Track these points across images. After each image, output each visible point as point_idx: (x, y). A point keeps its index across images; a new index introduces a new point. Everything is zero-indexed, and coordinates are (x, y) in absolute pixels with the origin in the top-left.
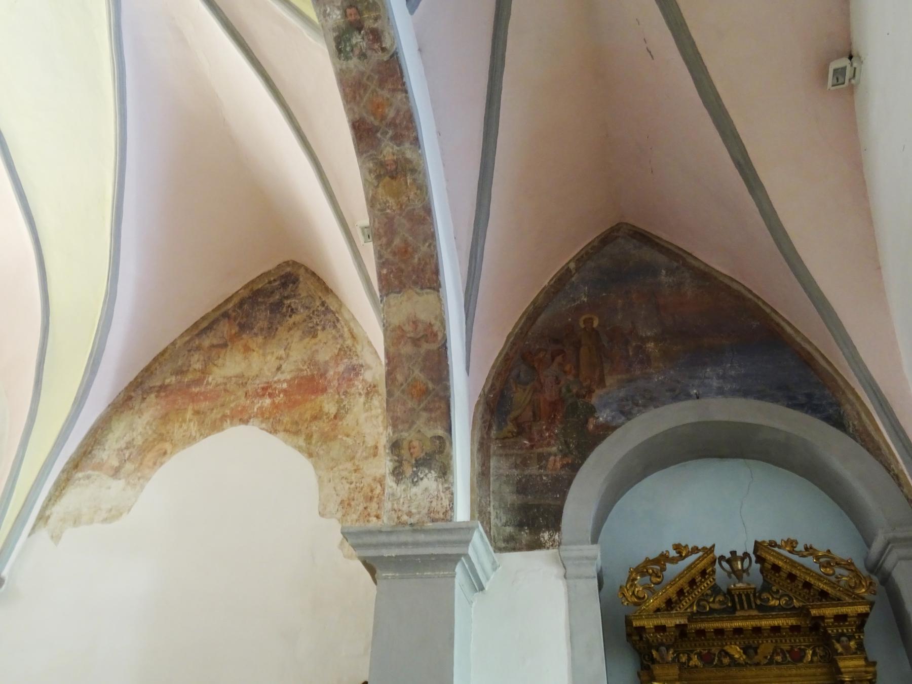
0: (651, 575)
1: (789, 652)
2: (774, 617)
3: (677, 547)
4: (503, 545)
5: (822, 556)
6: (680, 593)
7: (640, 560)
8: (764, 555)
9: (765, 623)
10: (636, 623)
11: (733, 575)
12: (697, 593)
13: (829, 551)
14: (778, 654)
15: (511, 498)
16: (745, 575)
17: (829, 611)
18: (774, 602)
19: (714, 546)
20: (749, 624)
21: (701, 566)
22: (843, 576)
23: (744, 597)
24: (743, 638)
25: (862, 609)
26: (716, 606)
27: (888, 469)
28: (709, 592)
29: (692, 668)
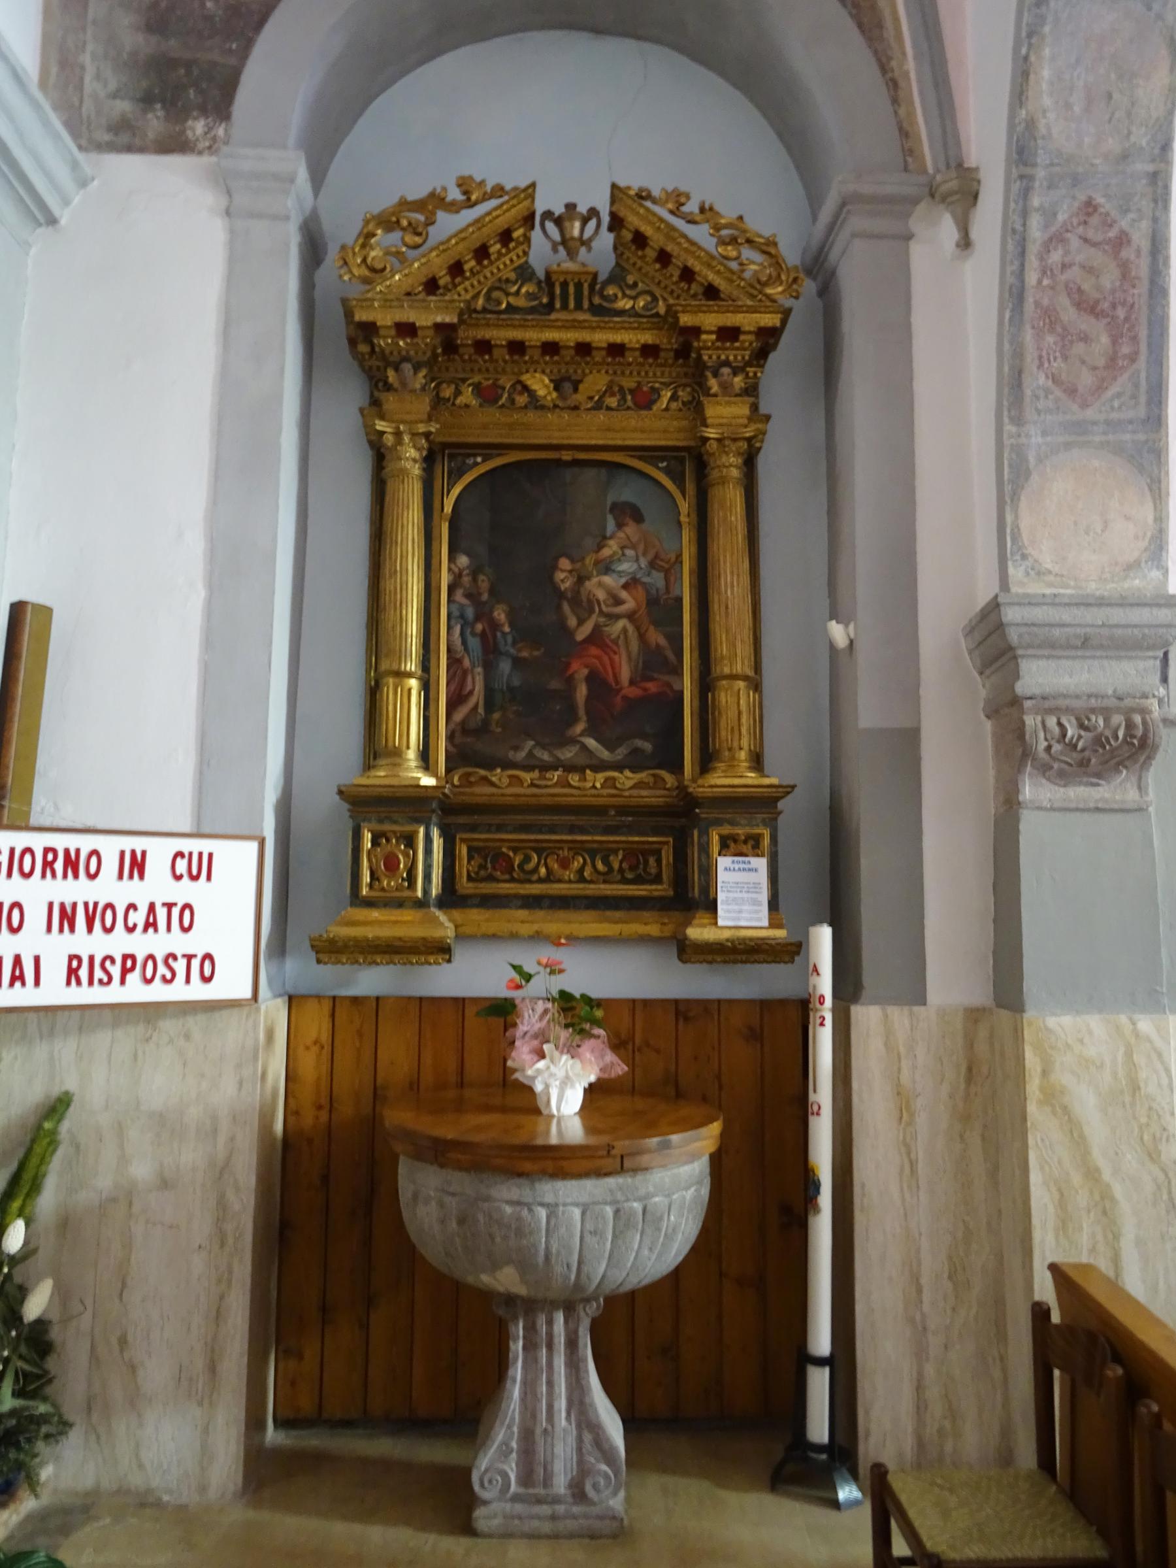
0: (403, 229)
1: (631, 391)
2: (615, 329)
3: (464, 184)
4: (107, 137)
5: (726, 226)
6: (456, 269)
7: (385, 201)
8: (623, 212)
9: (600, 338)
10: (361, 316)
11: (561, 248)
12: (490, 273)
13: (741, 218)
14: (613, 395)
15: (133, 40)
16: (583, 250)
17: (711, 320)
18: (625, 304)
19: (614, 186)
20: (569, 337)
21: (502, 223)
22: (753, 263)
23: (571, 289)
24: (557, 363)
25: (770, 320)
26: (521, 302)
27: (884, 68)
28: (512, 276)
29: (460, 407)
